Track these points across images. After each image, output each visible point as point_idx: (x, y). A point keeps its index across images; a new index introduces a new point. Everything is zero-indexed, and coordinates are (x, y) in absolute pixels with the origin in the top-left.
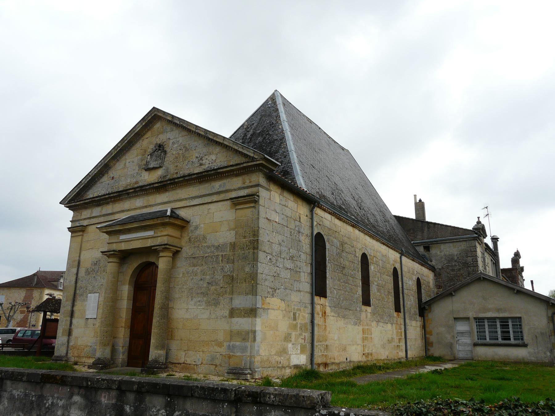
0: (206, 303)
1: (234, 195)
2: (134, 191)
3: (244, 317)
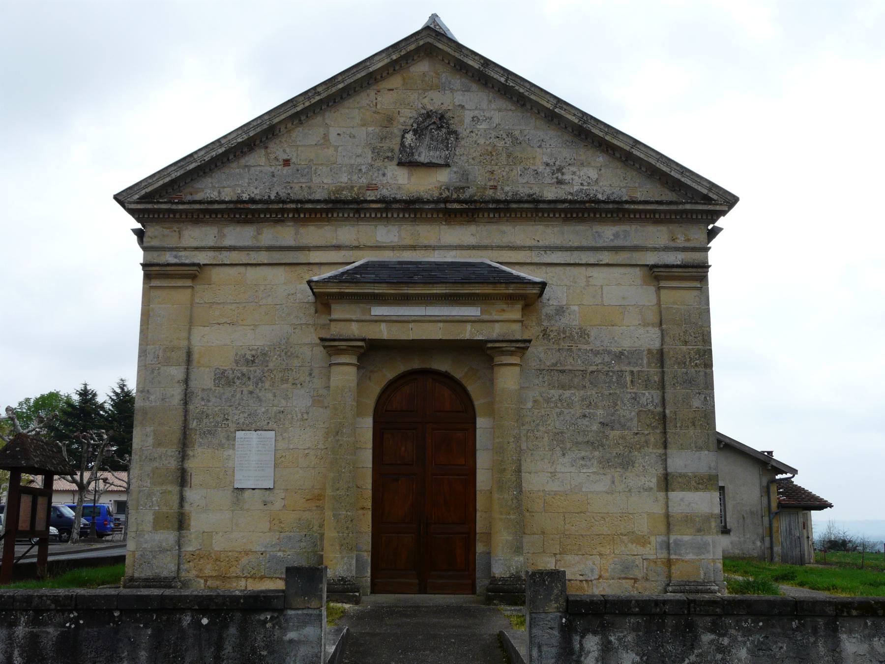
0: (600, 462)
1: (651, 259)
3: (697, 489)
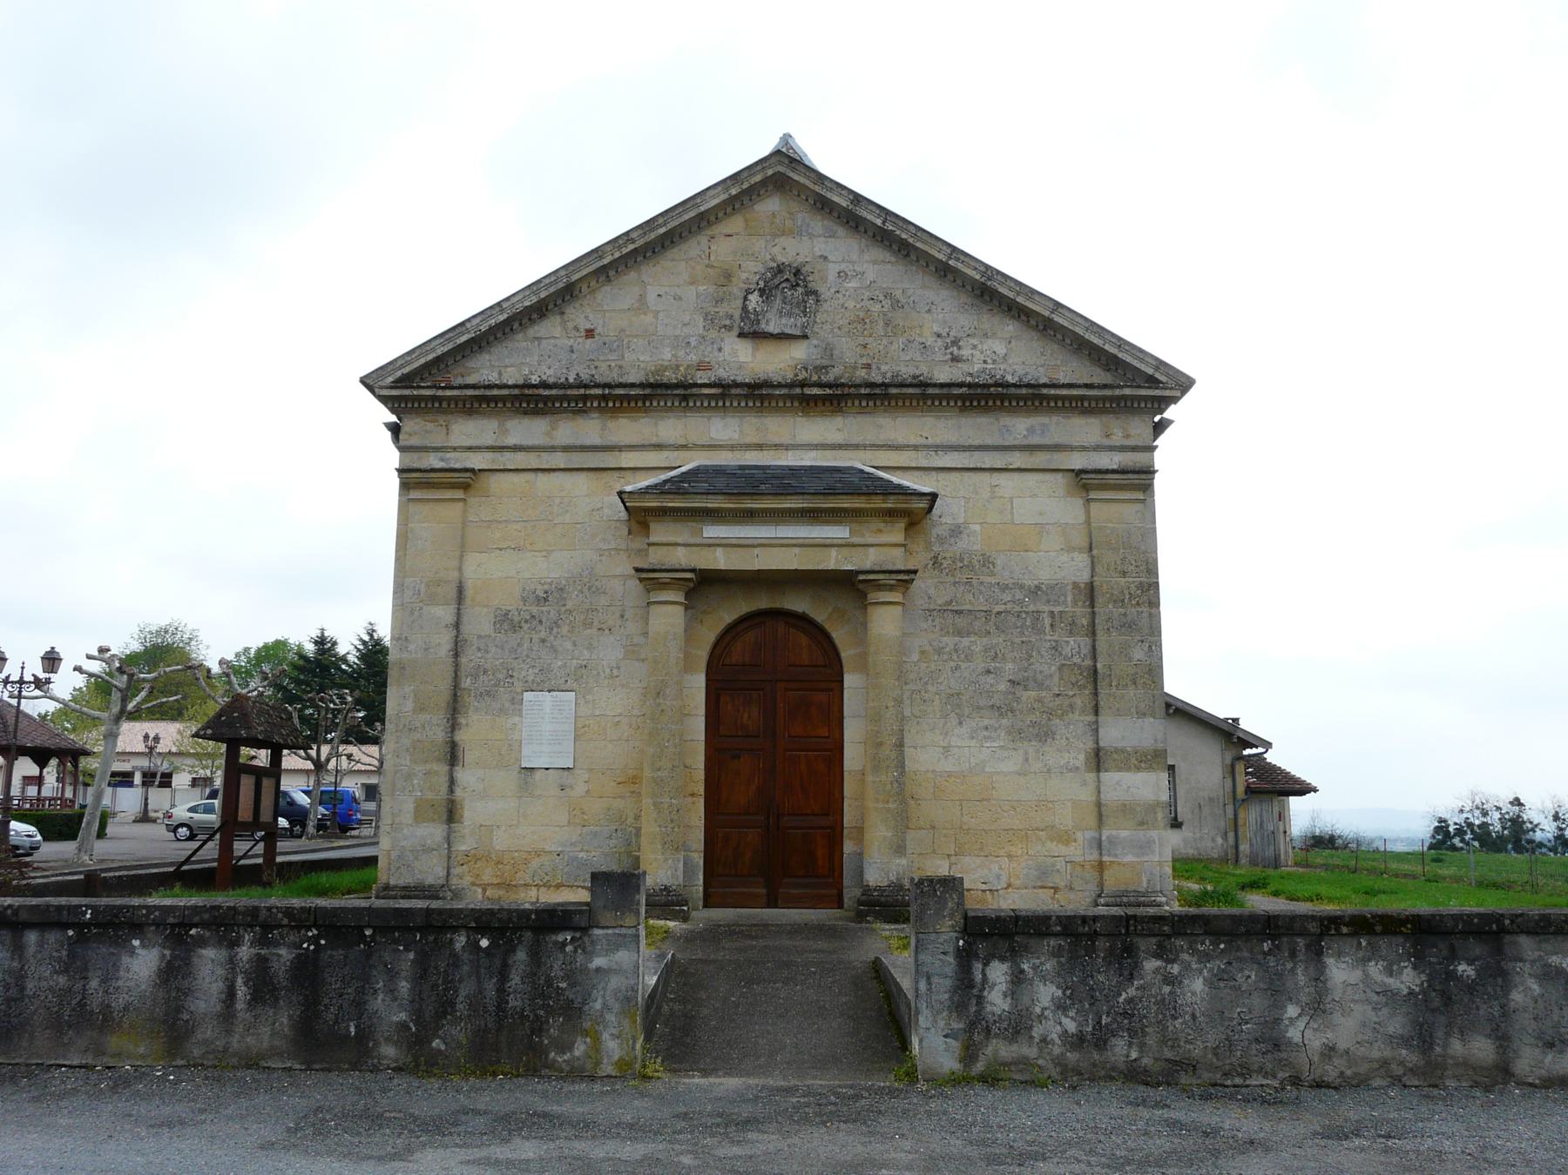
0: (1010, 733)
1: (1078, 461)
2: (721, 394)
3: (1138, 769)
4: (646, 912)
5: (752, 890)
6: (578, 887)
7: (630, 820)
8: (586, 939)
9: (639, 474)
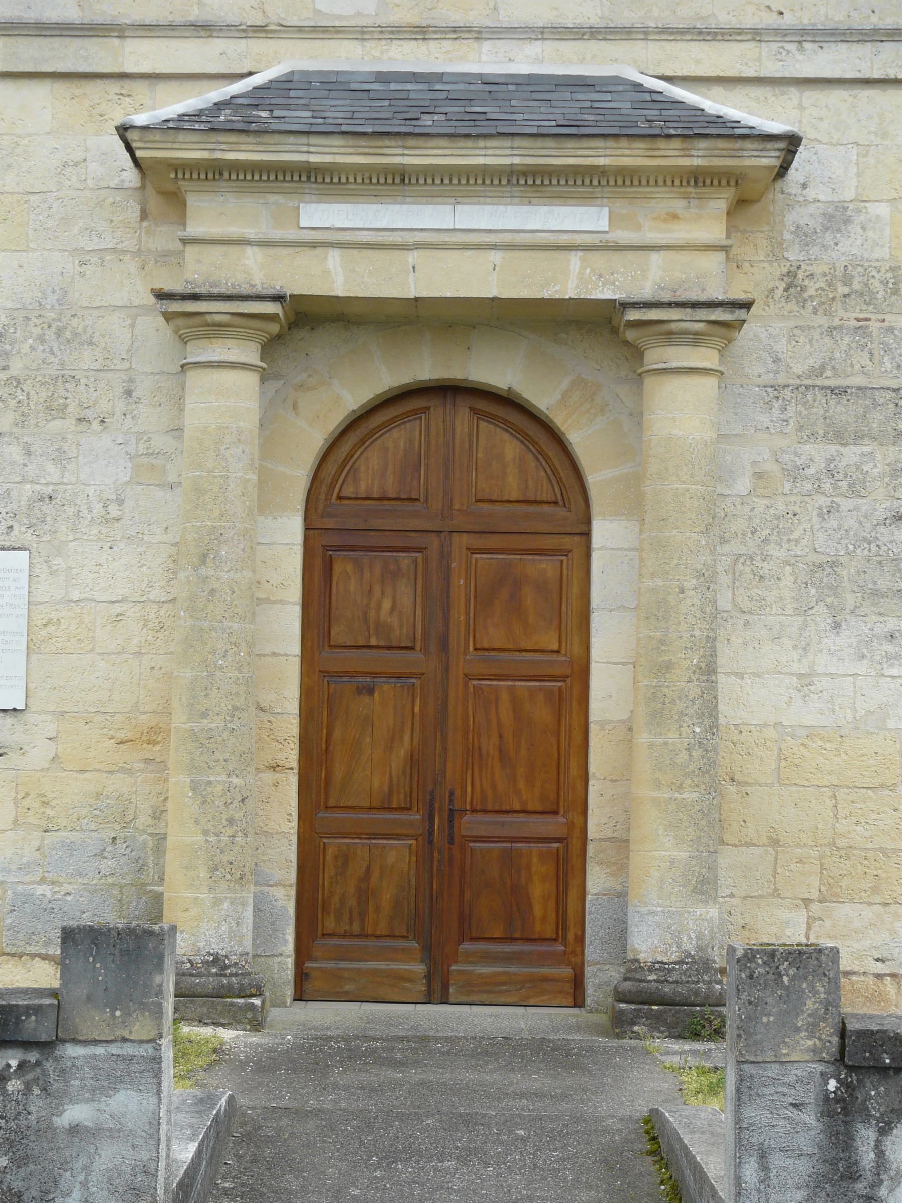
4: (176, 1009)
5: (394, 966)
6: (33, 956)
7: (144, 820)
8: (49, 1065)
9: (163, 89)
